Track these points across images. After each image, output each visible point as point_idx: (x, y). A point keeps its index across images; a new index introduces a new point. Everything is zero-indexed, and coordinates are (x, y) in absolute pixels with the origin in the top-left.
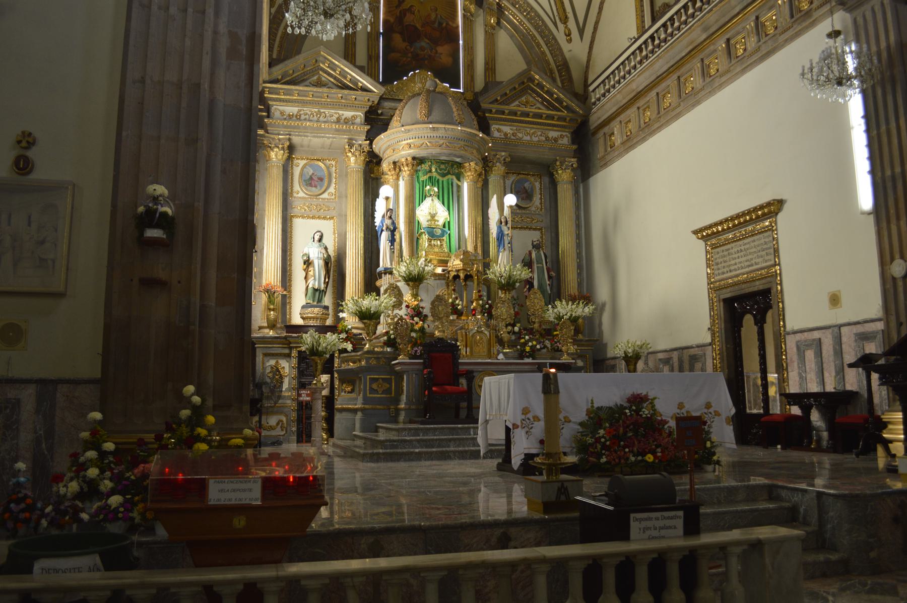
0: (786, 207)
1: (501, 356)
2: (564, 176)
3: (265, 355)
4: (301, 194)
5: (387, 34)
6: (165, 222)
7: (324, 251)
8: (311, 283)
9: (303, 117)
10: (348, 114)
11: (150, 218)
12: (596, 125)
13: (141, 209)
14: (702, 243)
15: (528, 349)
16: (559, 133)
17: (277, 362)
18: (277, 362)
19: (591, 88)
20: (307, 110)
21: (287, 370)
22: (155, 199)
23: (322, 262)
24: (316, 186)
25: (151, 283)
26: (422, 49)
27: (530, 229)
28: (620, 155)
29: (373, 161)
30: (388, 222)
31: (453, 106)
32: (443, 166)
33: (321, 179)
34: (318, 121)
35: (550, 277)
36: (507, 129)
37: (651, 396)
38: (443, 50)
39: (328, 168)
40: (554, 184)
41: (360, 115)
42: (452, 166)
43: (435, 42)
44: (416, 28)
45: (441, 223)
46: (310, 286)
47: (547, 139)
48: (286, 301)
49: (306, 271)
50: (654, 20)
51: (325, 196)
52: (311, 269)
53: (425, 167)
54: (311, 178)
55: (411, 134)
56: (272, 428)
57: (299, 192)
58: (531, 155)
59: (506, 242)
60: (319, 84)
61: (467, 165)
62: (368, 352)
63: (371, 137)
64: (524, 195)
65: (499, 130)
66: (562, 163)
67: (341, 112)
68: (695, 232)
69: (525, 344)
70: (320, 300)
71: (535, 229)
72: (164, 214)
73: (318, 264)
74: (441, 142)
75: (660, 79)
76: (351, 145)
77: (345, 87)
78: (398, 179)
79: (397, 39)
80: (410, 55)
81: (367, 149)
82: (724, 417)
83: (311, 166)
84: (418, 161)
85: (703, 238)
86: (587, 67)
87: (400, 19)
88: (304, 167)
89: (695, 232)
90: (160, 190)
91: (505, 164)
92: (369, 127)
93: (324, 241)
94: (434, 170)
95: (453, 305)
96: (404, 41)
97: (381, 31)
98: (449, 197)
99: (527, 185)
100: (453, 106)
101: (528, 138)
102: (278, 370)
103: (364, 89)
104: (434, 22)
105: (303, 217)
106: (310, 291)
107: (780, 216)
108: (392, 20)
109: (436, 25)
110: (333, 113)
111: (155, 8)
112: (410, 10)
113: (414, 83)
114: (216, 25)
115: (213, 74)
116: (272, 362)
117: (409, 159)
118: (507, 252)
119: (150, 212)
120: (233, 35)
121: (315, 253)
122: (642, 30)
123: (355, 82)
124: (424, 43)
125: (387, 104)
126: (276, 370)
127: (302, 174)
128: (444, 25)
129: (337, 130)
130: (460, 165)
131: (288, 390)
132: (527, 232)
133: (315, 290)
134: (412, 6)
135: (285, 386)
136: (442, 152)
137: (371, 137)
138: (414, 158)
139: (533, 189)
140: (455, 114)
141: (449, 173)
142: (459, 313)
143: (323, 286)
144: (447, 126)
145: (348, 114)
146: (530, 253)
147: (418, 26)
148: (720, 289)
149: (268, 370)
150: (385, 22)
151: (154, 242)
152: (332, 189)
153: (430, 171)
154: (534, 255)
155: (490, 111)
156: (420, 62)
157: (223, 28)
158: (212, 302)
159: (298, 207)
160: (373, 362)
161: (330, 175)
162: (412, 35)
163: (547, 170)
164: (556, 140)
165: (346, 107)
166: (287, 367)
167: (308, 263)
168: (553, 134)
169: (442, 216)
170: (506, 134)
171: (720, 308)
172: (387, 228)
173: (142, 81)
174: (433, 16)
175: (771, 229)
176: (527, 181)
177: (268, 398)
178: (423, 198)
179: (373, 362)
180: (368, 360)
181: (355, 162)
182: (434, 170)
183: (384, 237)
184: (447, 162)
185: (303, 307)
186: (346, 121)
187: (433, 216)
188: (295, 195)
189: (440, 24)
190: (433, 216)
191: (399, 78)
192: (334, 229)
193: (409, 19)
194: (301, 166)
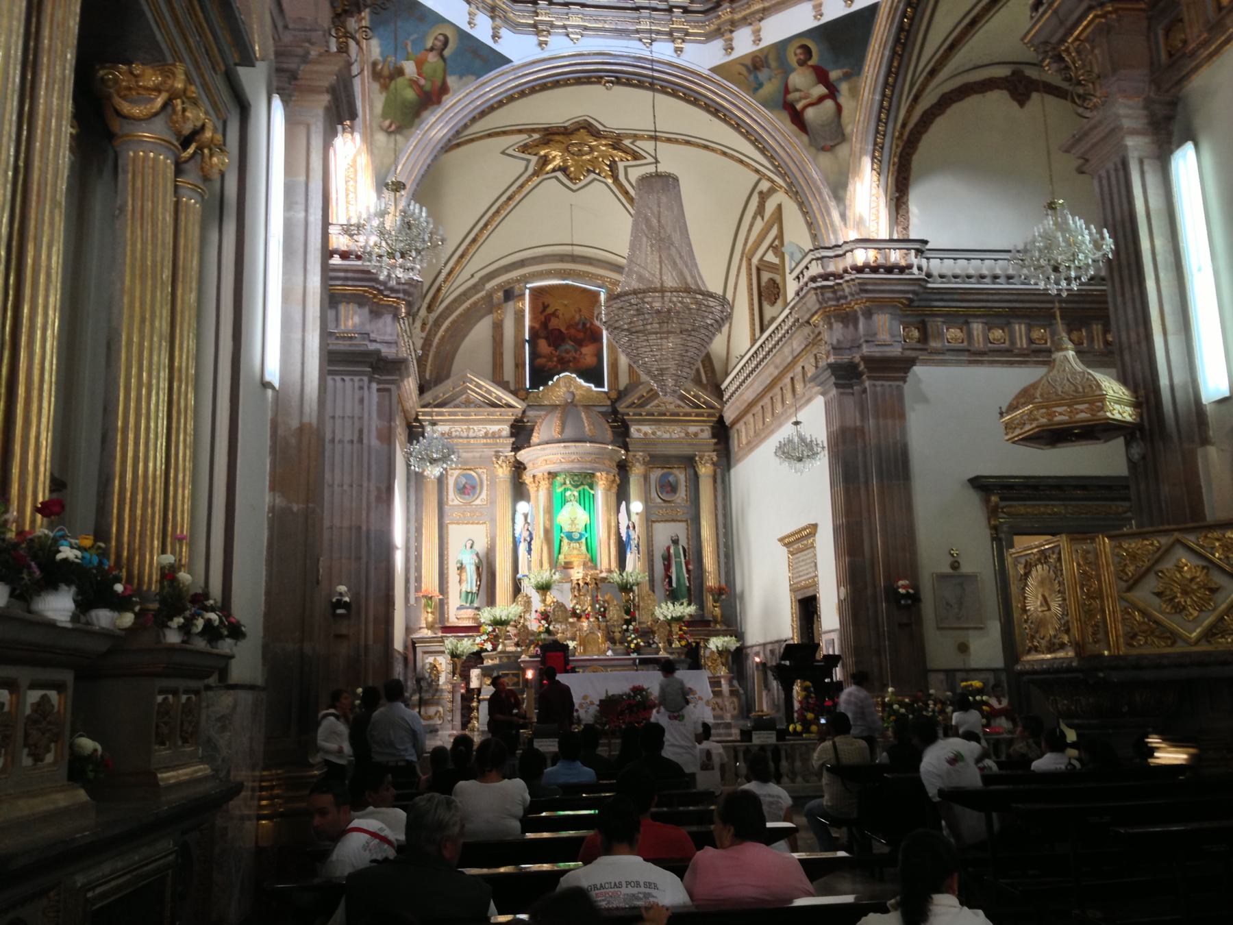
0: (819, 529)
1: (609, 653)
2: (705, 470)
3: (425, 653)
4: (456, 502)
5: (533, 341)
6: (346, 605)
7: (475, 557)
8: (466, 587)
9: (454, 434)
10: (494, 428)
11: (340, 604)
12: (731, 420)
13: (334, 600)
14: (785, 549)
15: (632, 646)
16: (699, 428)
17: (435, 659)
18: (435, 659)
19: (723, 387)
20: (458, 427)
21: (444, 666)
22: (341, 594)
23: (473, 568)
24: (469, 494)
25: (339, 637)
26: (567, 352)
27: (673, 521)
28: (746, 455)
29: (519, 468)
30: (526, 534)
31: (585, 421)
32: (576, 478)
33: (474, 488)
34: (468, 437)
35: (688, 571)
36: (647, 429)
37: (645, 687)
38: (587, 350)
39: (479, 475)
40: (695, 479)
41: (506, 429)
42: (585, 477)
43: (579, 343)
44: (560, 331)
45: (581, 527)
46: (464, 590)
47: (687, 434)
48: (442, 604)
49: (460, 575)
50: (762, 330)
51: (478, 502)
52: (464, 574)
53: (559, 479)
54: (464, 487)
55: (548, 451)
56: (430, 718)
57: (453, 498)
58: (672, 451)
59: (633, 546)
60: (468, 403)
61: (598, 474)
62: (500, 652)
63: (516, 448)
64: (669, 489)
65: (639, 431)
66: (701, 458)
67: (488, 427)
68: (781, 540)
69: (631, 641)
70: (472, 602)
71: (680, 521)
72: (346, 602)
73: (471, 571)
74: (573, 457)
75: (760, 397)
76: (498, 457)
77: (494, 405)
78: (538, 490)
79: (543, 346)
80: (555, 359)
81: (512, 460)
82: (705, 700)
83: (464, 475)
84: (552, 475)
85: (785, 545)
86: (727, 358)
87: (545, 325)
88: (458, 477)
89: (781, 540)
90: (343, 588)
91: (645, 463)
92: (513, 439)
93: (475, 547)
94: (568, 482)
95: (574, 610)
96: (549, 345)
97: (527, 338)
98: (586, 501)
99: (671, 479)
100: (585, 421)
101: (667, 436)
102: (435, 666)
103: (510, 406)
104: (577, 324)
105: (458, 524)
106: (464, 595)
107: (817, 535)
108: (537, 326)
109: (580, 326)
110: (480, 430)
111: (336, 487)
112: (554, 314)
113: (559, 387)
114: (368, 487)
115: (368, 516)
116: (430, 659)
117: (546, 474)
118: (633, 555)
119: (339, 601)
120: (378, 489)
121: (470, 561)
122: (754, 341)
123: (500, 399)
124: (569, 345)
125: (530, 413)
126: (434, 667)
127: (456, 483)
128: (588, 325)
129: (485, 444)
130: (592, 475)
131: (445, 683)
132: (672, 524)
133: (467, 593)
134: (556, 310)
135: (442, 680)
136: (576, 467)
137: (516, 448)
138: (549, 473)
139: (677, 482)
140: (587, 429)
141: (582, 484)
142: (579, 617)
143: (475, 589)
144: (577, 444)
145: (494, 428)
146: (668, 549)
147: (563, 329)
148: (799, 590)
149: (428, 666)
150: (532, 329)
151: (341, 615)
152: (484, 495)
153: (565, 484)
154: (672, 551)
155: (628, 415)
156: (564, 365)
157: (373, 488)
158: (371, 642)
159: (450, 514)
160: (505, 660)
161: (481, 481)
162: (556, 338)
163: (689, 462)
164: (696, 435)
165: (493, 422)
166: (443, 663)
167: (461, 568)
168: (692, 429)
169: (582, 517)
170: (645, 434)
171: (796, 606)
172: (525, 540)
173: (331, 528)
174: (577, 317)
175: (812, 546)
176: (671, 474)
177: (427, 691)
178: (565, 501)
179: (505, 660)
180: (500, 658)
181: (503, 472)
182: (568, 482)
183: (522, 548)
184: (581, 474)
185: (459, 609)
186: (494, 436)
187: (573, 522)
188: (450, 503)
189: (584, 325)
190: (573, 522)
191: (545, 384)
192: (638, 884)
193: (554, 323)
194: (455, 476)
